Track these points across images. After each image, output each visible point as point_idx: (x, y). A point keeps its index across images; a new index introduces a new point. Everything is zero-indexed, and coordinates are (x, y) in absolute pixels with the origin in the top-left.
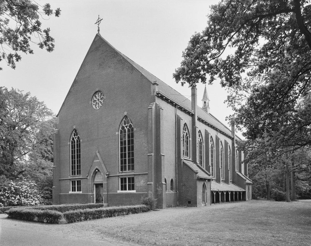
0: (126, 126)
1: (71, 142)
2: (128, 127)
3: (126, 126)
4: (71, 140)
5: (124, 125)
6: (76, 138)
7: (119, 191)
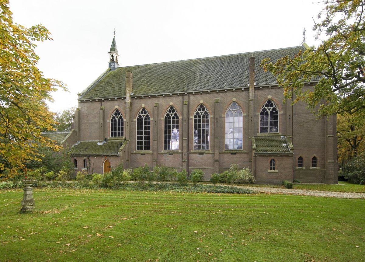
2: (118, 118)
4: (137, 117)
5: (115, 116)
7: (311, 168)
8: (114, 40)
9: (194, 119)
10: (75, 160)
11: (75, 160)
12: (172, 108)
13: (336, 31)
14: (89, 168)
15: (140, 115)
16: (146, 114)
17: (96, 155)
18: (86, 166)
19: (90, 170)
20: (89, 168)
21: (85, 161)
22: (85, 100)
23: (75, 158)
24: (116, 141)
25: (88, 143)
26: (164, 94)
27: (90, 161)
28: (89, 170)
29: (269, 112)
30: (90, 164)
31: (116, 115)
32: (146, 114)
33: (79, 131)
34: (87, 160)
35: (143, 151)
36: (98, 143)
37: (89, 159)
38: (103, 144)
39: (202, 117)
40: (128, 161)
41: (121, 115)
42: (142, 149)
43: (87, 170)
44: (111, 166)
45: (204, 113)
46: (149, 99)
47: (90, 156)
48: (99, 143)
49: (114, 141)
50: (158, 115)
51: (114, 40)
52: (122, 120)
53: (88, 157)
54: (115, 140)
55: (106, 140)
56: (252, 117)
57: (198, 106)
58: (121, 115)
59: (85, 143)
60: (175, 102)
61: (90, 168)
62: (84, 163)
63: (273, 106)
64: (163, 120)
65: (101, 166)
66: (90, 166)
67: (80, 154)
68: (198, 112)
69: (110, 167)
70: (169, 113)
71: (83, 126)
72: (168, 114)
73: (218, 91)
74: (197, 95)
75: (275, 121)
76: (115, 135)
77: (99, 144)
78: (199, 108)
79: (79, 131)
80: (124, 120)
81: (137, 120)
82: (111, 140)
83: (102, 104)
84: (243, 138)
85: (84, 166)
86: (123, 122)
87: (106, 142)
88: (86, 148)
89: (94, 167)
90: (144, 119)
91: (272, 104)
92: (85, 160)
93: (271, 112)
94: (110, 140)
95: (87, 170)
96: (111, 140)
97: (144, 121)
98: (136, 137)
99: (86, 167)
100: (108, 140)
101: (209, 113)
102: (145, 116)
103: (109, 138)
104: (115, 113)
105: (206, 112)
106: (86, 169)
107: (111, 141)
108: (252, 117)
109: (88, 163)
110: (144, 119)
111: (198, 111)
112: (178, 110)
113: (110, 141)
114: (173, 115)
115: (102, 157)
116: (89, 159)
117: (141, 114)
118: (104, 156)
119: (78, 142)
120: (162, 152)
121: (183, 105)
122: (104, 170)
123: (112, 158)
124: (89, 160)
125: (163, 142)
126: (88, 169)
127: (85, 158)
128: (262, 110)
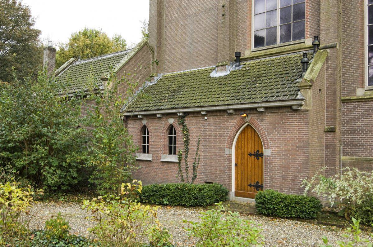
10: (144, 130)
11: (144, 130)
13: (90, 201)
14: (184, 157)
17: (208, 109)
18: (175, 147)
19: (186, 164)
20: (184, 157)
21: (171, 133)
23: (144, 122)
24: (274, 58)
25: (182, 75)
27: (187, 130)
28: (183, 164)
30: (187, 142)
33: (159, 43)
34: (179, 129)
36: (214, 71)
37: (183, 124)
38: (228, 73)
40: (332, 131)
43: (179, 163)
44: (267, 152)
47: (186, 114)
48: (217, 71)
49: (268, 59)
50: (222, 66)
53: (182, 117)
54: (272, 55)
55: (238, 58)
59: (173, 78)
61: (186, 157)
62: (171, 138)
65: (227, 151)
66: (187, 151)
67: (158, 110)
69: (262, 155)
71: (169, 31)
77: (214, 74)
79: (159, 43)
82: (257, 57)
85: (170, 148)
87: (239, 65)
88: (177, 91)
89: (200, 153)
92: (171, 129)
94: (251, 58)
95: (179, 163)
96: (257, 57)
98: (363, 30)
99: (175, 154)
100: (245, 59)
103: (247, 54)
106: (174, 158)
107: (258, 61)
109: (180, 140)
113: (252, 62)
115: (231, 114)
116: (183, 124)
118: (236, 110)
119: (157, 76)
122: (236, 165)
123: (269, 118)
124: (185, 129)
125: (248, 200)
126: (180, 159)
127: (171, 121)
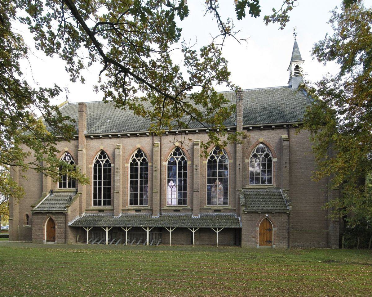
0: (176, 158)
1: (167, 162)
3: (218, 158)
6: (102, 161)
8: (296, 46)
9: (207, 164)
12: (139, 151)
15: (98, 160)
16: (142, 158)
22: (102, 135)
26: (197, 129)
29: (177, 162)
31: (138, 157)
32: (142, 158)
35: (102, 207)
39: (140, 166)
41: (145, 157)
42: (100, 204)
45: (105, 162)
46: (128, 139)
51: (296, 46)
52: (110, 165)
56: (239, 164)
57: (135, 151)
58: (145, 157)
60: (145, 143)
63: (143, 156)
64: (91, 168)
68: (212, 155)
70: (214, 155)
72: (98, 160)
73: (177, 132)
74: (191, 135)
75: (267, 170)
76: (65, 186)
78: (100, 156)
80: (112, 165)
81: (208, 163)
83: (162, 139)
84: (166, 194)
86: (186, 166)
90: (102, 165)
91: (105, 155)
93: (220, 159)
97: (218, 164)
101: (187, 159)
102: (104, 162)
104: (214, 150)
105: (144, 159)
108: (239, 164)
110: (102, 165)
111: (255, 152)
112: (147, 155)
114: (104, 162)
115: (53, 214)
117: (135, 158)
120: (205, 207)
121: (153, 147)
128: (96, 162)
